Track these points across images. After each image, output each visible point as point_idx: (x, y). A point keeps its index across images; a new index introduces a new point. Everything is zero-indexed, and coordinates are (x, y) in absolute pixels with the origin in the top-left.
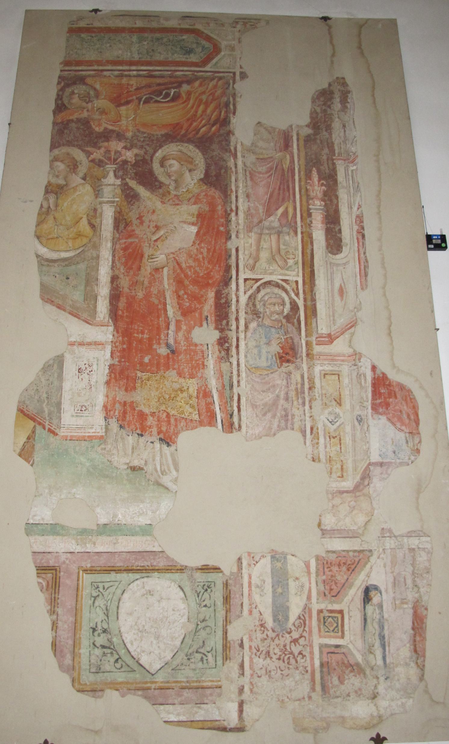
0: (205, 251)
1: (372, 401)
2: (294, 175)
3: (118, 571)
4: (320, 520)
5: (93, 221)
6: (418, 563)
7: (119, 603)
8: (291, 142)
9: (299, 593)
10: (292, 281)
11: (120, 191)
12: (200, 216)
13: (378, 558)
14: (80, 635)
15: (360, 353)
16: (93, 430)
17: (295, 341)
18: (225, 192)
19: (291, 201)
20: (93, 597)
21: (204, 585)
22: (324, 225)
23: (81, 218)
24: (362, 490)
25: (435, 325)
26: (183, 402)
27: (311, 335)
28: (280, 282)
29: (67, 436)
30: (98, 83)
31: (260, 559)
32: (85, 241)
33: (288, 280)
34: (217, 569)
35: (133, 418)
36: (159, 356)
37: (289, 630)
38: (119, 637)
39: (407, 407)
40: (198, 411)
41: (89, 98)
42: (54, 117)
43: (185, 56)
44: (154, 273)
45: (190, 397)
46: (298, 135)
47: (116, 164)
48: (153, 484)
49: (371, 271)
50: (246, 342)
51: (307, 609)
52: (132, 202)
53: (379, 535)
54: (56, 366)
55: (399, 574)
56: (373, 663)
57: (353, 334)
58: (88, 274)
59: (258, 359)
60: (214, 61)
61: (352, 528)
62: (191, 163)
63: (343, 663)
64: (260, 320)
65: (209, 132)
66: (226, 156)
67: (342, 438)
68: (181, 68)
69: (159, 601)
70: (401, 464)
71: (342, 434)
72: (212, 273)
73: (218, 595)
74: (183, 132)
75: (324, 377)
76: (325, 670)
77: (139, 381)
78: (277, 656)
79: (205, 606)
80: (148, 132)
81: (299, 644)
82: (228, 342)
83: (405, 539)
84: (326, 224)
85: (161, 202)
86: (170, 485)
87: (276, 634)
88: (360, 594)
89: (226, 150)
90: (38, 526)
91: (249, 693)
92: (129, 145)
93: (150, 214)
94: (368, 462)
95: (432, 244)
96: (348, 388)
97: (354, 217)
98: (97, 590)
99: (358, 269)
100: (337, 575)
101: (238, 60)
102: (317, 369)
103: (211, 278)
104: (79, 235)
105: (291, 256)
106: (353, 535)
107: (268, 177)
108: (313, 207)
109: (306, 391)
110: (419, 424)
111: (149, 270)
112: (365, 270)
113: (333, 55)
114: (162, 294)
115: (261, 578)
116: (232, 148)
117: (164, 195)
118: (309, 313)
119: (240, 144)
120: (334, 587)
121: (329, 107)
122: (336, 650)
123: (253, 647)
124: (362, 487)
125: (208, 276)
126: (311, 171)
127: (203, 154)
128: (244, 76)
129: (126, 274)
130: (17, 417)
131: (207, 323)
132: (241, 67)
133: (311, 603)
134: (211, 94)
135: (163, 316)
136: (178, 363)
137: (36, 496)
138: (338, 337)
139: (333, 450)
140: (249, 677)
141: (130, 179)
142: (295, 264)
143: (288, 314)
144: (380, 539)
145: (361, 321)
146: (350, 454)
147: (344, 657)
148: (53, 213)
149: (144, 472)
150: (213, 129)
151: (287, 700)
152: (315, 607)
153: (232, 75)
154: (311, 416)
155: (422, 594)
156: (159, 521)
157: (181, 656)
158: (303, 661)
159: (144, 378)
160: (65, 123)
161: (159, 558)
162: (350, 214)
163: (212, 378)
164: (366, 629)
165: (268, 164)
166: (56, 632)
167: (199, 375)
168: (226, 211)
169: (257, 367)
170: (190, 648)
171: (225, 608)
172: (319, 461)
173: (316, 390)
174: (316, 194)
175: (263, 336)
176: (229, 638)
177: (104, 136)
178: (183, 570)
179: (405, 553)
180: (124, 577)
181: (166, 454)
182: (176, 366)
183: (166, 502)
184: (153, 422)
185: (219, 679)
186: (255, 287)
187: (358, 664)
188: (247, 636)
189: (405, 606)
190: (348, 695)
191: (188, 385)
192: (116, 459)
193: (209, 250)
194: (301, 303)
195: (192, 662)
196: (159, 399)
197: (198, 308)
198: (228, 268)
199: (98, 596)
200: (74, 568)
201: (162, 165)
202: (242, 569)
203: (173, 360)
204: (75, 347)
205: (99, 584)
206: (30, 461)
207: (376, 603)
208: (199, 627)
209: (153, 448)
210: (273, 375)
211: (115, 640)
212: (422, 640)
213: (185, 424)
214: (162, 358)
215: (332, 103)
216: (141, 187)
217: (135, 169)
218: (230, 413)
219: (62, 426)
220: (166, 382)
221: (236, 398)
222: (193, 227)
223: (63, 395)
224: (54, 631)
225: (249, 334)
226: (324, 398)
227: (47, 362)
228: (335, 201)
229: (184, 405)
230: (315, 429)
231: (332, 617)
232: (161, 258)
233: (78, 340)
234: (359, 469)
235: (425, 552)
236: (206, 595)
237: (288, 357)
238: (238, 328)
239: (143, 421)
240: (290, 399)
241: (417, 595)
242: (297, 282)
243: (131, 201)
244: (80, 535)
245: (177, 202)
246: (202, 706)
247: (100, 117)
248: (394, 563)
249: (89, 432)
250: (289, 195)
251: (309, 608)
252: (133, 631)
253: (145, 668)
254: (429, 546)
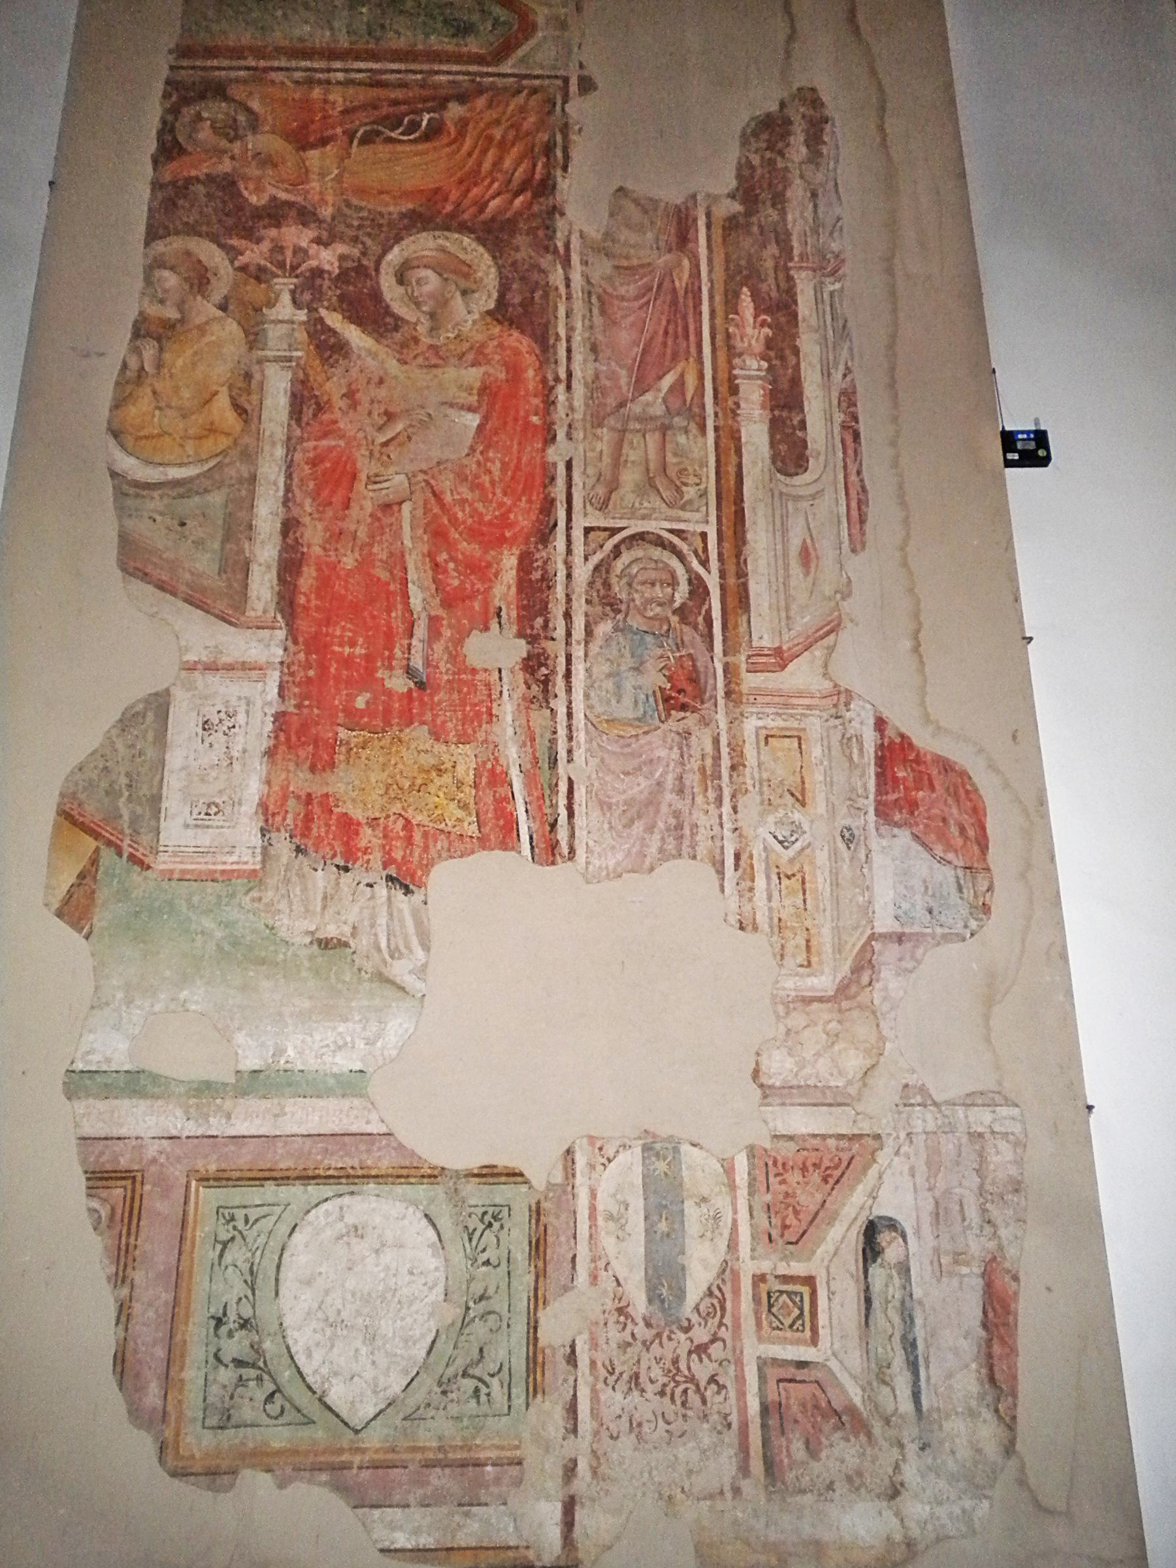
0: (496, 468)
1: (877, 796)
2: (701, 304)
3: (283, 1179)
4: (757, 1063)
5: (242, 401)
6: (992, 1167)
7: (281, 1255)
8: (692, 231)
9: (708, 1234)
10: (694, 533)
11: (305, 334)
13: (897, 1153)
14: (183, 1334)
15: (847, 690)
16: (234, 858)
17: (699, 664)
18: (543, 340)
19: (691, 360)
20: (219, 1242)
21: (485, 1213)
22: (768, 412)
23: (216, 393)
24: (854, 997)
25: (1023, 630)
26: (441, 795)
27: (736, 652)
28: (666, 535)
29: (172, 871)
30: (257, 96)
31: (618, 1152)
32: (224, 442)
33: (683, 531)
34: (515, 1175)
35: (327, 832)
36: (389, 693)
37: (686, 1324)
38: (279, 1337)
39: (959, 809)
40: (477, 816)
41: (236, 130)
42: (155, 170)
43: (455, 41)
44: (379, 514)
45: (460, 785)
46: (708, 215)
47: (297, 277)
48: (371, 980)
49: (873, 511)
50: (588, 665)
51: (727, 1271)
52: (331, 361)
53: (898, 1101)
54: (150, 716)
55: (948, 1192)
56: (890, 1408)
57: (831, 649)
58: (229, 517)
59: (613, 702)
60: (520, 52)
61: (832, 1084)
62: (466, 276)
63: (817, 1407)
64: (620, 617)
65: (506, 210)
66: (545, 261)
67: (807, 878)
68: (445, 68)
69: (377, 1251)
70: (946, 938)
71: (806, 868)
72: (512, 516)
73: (517, 1237)
74: (449, 208)
75: (767, 743)
76: (773, 1422)
77: (343, 749)
78: (658, 1387)
79: (487, 1263)
80: (369, 206)
81: (709, 1357)
82: (546, 665)
83: (960, 1111)
84: (772, 410)
85: (398, 360)
86: (409, 981)
87: (654, 1332)
88: (855, 1238)
89: (547, 249)
90: (96, 1076)
91: (588, 1476)
92: (325, 235)
93: (372, 386)
94: (869, 932)
95: (1015, 450)
96: (822, 768)
97: (835, 394)
98: (230, 1227)
99: (845, 507)
100: (798, 1192)
101: (576, 49)
102: (751, 725)
103: (510, 526)
104: (212, 430)
105: (692, 480)
106: (837, 1100)
107: (640, 308)
108: (744, 372)
109: (725, 773)
110: (987, 847)
111: (369, 506)
112: (859, 509)
113: (791, 38)
114: (398, 561)
115: (618, 1196)
116: (560, 244)
117: (404, 345)
118: (731, 602)
119: (578, 234)
120: (791, 1220)
121: (781, 153)
122: (800, 1375)
123: (599, 1364)
124: (854, 989)
125: (504, 521)
126: (737, 295)
127: (494, 258)
128: (587, 86)
129: (316, 516)
130: (57, 828)
131: (500, 623)
132: (581, 66)
133: (738, 1259)
134: (512, 126)
135: (400, 607)
136: (432, 709)
137: (93, 1007)
138: (798, 656)
139: (788, 906)
140: (589, 1438)
141: (327, 308)
142: (701, 496)
143: (683, 605)
144: (901, 1108)
145: (852, 621)
146: (828, 913)
147: (818, 1393)
148: (148, 381)
149: (349, 951)
151: (679, 1496)
152: (748, 1268)
153: (559, 82)
154: (736, 829)
155: (1005, 1243)
156: (381, 1063)
157: (428, 1381)
158: (720, 1398)
159: (354, 741)
160: (180, 183)
161: (379, 1149)
162: (827, 386)
163: (510, 744)
164: (871, 1323)
165: (641, 279)
166: (126, 1329)
167: (481, 735)
168: (544, 381)
169: (613, 721)
170: (447, 1365)
171: (532, 1268)
172: (755, 928)
173: (748, 771)
174: (750, 345)
175: (627, 653)
176: (541, 1343)
177: (269, 215)
178: (435, 1177)
179: (960, 1145)
180: (295, 1193)
181: (400, 911)
182: (428, 717)
183: (399, 1021)
184: (374, 840)
185: (517, 1443)
186: (609, 545)
187: (852, 1410)
188: (586, 1336)
189: (965, 1270)
190: (830, 1487)
191: (454, 759)
192: (286, 921)
193: (505, 466)
194: (712, 581)
195: (452, 1401)
196: (387, 789)
197: (478, 590)
198: (548, 505)
199: (233, 1238)
200: (177, 1173)
201: (401, 280)
202: (574, 1175)
203: (422, 704)
204: (196, 673)
205: (235, 1211)
206: (83, 929)
207: (893, 1261)
208: (472, 1314)
209: (372, 897)
210: (648, 737)
211: (267, 1345)
212: (1008, 1355)
213: (446, 845)
214: (395, 698)
215: (788, 145)
216: (353, 327)
217: (340, 288)
218: (551, 820)
219: (162, 849)
220: (404, 753)
221: (563, 787)
222: (470, 416)
223: (165, 781)
224: (120, 1326)
225: (594, 648)
226: (765, 789)
227: (132, 706)
228: (792, 360)
229: (445, 802)
230: (744, 857)
231: (789, 1294)
232: (398, 481)
233: (204, 659)
234: (848, 947)
235: (1008, 1141)
236: (489, 1237)
237: (683, 699)
238: (569, 634)
239: (349, 838)
240: (687, 791)
241: (991, 1245)
242: (704, 535)
243: (331, 357)
244: (194, 1097)
245: (434, 361)
246: (475, 1509)
247: (258, 173)
248: (934, 1165)
249: (225, 863)
250: (688, 347)
251: (732, 1270)
252: (314, 1324)
253: (338, 1416)
254: (1017, 1128)
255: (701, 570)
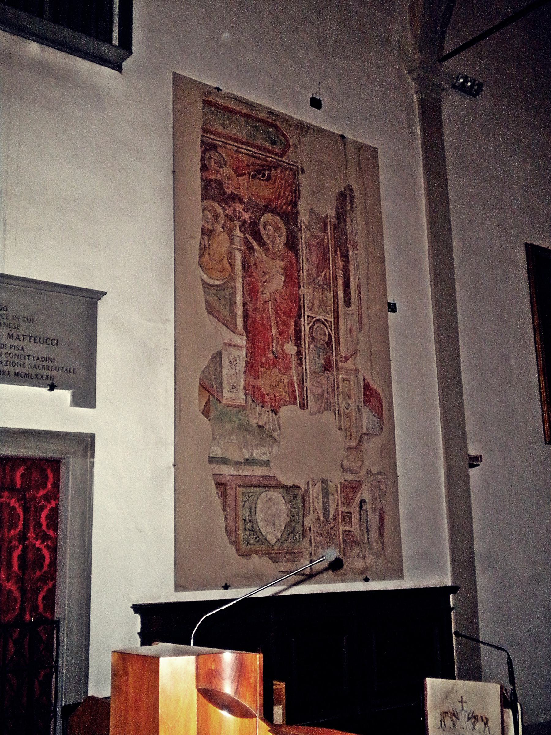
3: (255, 486)
4: (342, 463)
12: (285, 269)
18: (297, 254)
45: (285, 386)
46: (330, 222)
51: (337, 511)
57: (355, 358)
70: (376, 435)
73: (299, 501)
77: (260, 373)
86: (276, 437)
102: (341, 376)
114: (269, 318)
143: (327, 341)
150: (289, 208)
152: (340, 510)
159: (263, 371)
162: (355, 282)
221: (305, 389)
242: (331, 322)
245: (274, 257)
255: (330, 331)
